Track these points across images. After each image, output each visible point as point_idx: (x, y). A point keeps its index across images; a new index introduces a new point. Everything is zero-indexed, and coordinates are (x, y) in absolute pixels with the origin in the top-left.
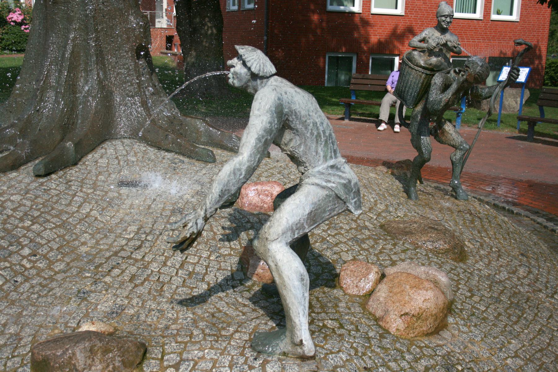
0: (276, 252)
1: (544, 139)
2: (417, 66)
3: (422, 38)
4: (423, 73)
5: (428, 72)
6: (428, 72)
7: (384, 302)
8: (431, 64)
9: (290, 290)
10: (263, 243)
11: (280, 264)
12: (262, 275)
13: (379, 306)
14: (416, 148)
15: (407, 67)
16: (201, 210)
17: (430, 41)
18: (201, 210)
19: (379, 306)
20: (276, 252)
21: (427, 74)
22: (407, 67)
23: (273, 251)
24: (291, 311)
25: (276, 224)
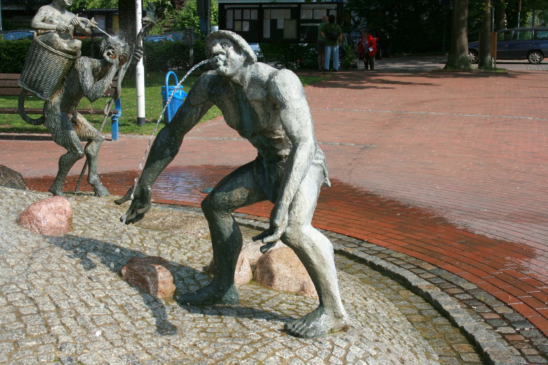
0: (309, 234)
1: (32, 135)
2: (59, 50)
3: (43, 18)
4: (66, 58)
5: (71, 57)
6: (71, 57)
7: (294, 277)
8: (75, 47)
9: (329, 267)
10: (296, 229)
11: (317, 244)
12: (164, 291)
13: (290, 282)
14: (65, 146)
15: (46, 52)
16: (287, 201)
17: (56, 21)
18: (287, 201)
19: (290, 282)
20: (309, 234)
21: (70, 59)
22: (46, 52)
23: (307, 234)
24: (331, 287)
25: (303, 207)
